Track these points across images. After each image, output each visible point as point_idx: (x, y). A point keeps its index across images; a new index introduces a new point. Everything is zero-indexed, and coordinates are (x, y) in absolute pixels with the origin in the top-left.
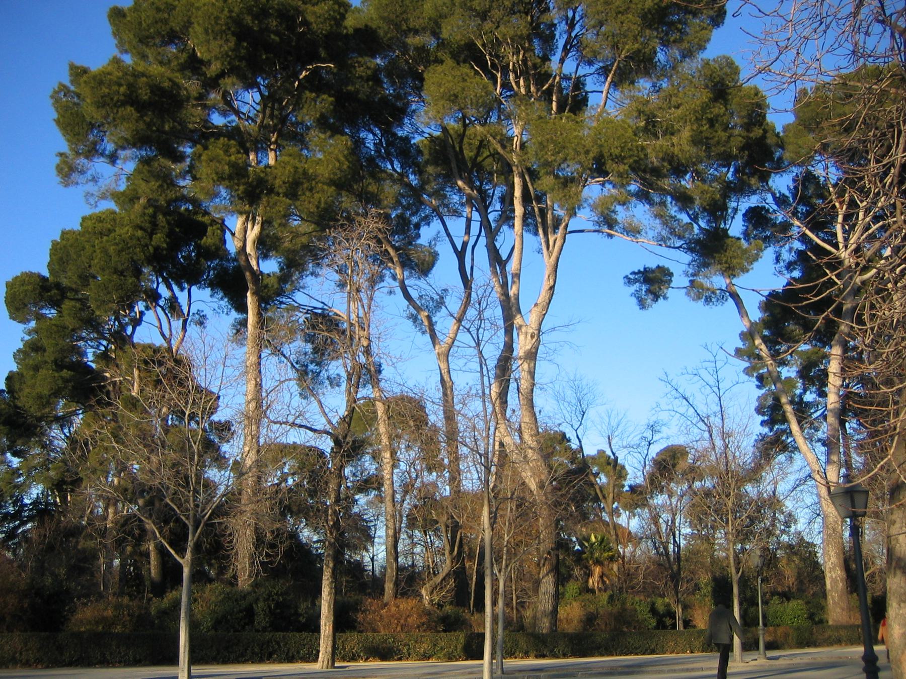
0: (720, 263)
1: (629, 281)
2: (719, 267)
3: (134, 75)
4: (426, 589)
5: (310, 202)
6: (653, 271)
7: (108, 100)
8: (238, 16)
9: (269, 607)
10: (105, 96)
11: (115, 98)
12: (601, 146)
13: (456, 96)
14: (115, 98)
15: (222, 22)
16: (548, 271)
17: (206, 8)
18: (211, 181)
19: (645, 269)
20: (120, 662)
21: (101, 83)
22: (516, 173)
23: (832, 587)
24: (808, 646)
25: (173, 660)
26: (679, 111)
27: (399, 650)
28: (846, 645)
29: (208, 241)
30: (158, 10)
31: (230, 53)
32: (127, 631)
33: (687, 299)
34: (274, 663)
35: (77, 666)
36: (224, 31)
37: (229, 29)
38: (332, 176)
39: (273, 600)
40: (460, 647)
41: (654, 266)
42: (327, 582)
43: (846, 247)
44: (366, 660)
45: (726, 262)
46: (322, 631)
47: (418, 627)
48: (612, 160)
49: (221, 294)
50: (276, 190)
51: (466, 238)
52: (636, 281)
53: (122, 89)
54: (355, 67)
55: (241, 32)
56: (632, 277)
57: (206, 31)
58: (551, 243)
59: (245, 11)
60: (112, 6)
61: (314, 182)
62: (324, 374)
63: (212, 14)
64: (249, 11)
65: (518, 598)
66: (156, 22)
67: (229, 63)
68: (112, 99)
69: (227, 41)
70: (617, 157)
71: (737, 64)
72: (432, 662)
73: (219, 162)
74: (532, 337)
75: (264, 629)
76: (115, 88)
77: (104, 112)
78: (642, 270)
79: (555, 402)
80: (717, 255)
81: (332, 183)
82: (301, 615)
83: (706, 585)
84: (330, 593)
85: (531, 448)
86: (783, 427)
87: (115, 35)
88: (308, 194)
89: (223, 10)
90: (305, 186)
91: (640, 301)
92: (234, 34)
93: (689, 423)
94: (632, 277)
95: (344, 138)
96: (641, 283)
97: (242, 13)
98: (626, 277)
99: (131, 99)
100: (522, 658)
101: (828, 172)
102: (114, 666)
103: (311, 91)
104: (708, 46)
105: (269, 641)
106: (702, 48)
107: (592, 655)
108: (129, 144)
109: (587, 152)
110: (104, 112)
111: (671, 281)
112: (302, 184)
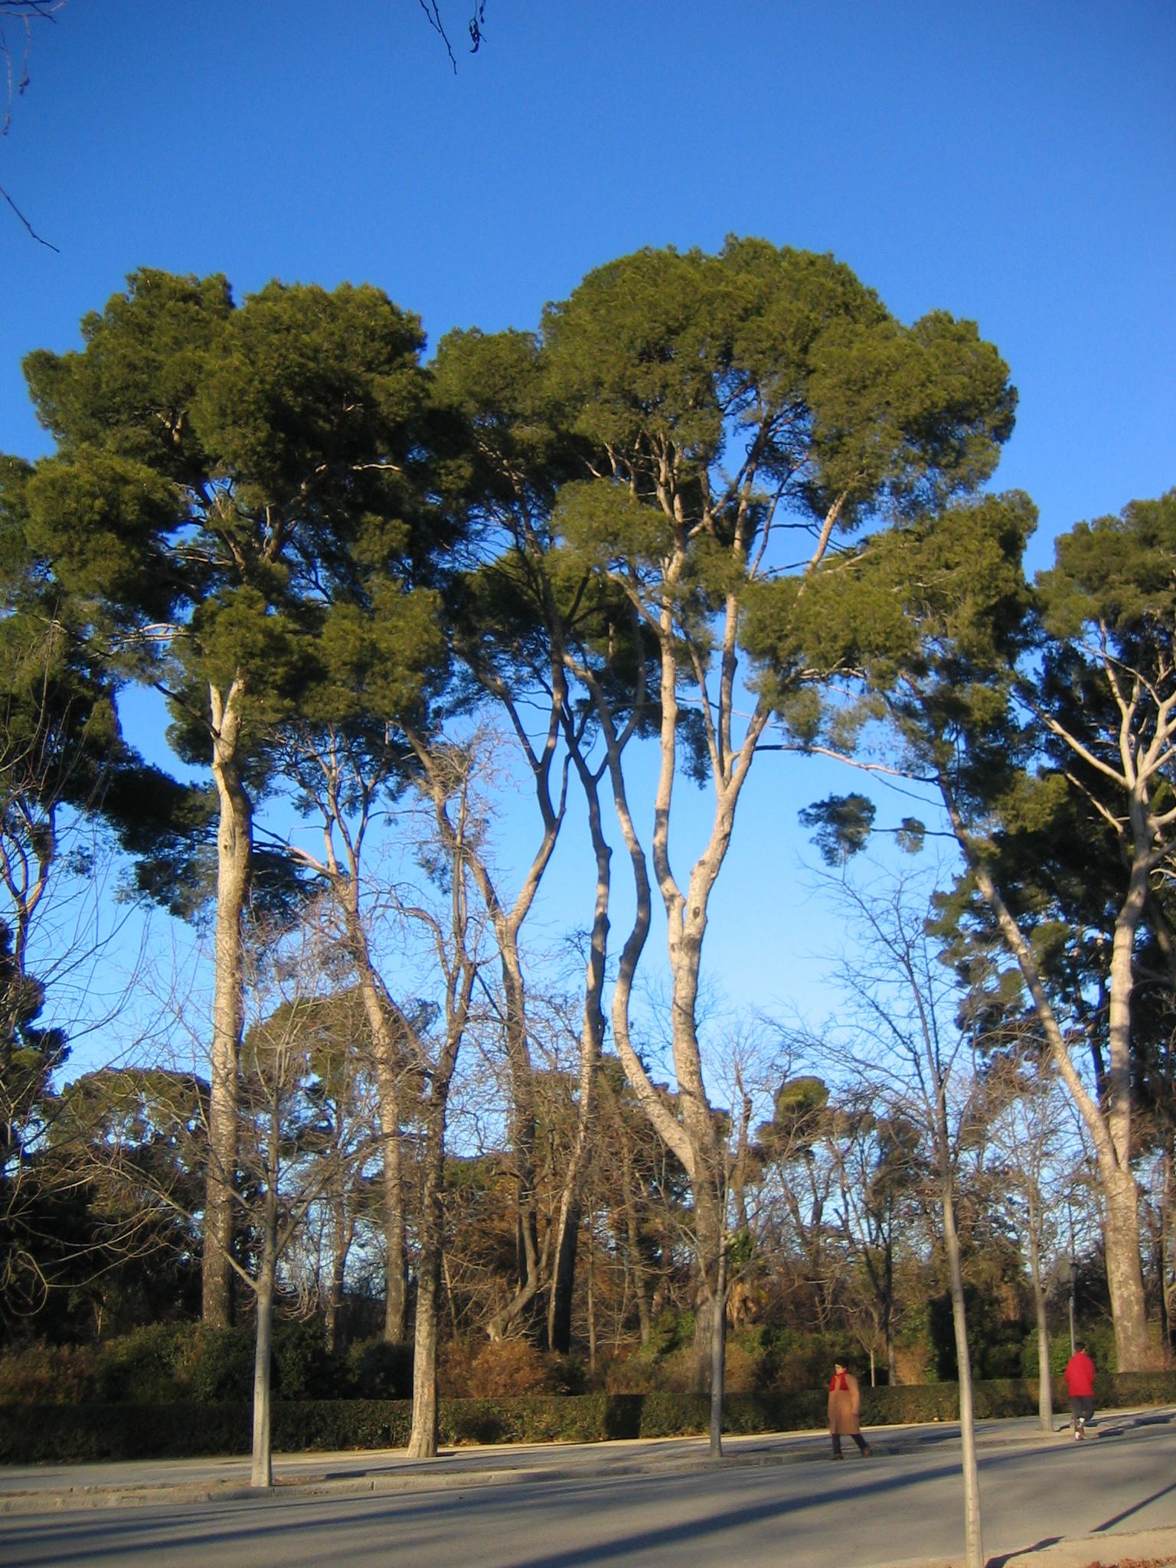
0: (1005, 809)
1: (808, 819)
2: (1003, 814)
3: (113, 480)
4: (495, 1326)
5: (384, 697)
6: (844, 803)
7: (74, 520)
8: (273, 389)
9: (304, 1357)
10: (71, 514)
11: (86, 518)
12: (855, 630)
13: (616, 535)
14: (86, 518)
15: (250, 397)
16: (721, 810)
17: (224, 373)
18: (233, 658)
19: (832, 798)
20: (75, 1456)
21: (64, 492)
22: (664, 649)
23: (1123, 1312)
24: (1107, 1407)
25: (244, 1448)
26: (954, 575)
27: (509, 1425)
28: (1160, 1403)
29: (91, 726)
30: (132, 367)
31: (259, 448)
32: (74, 1403)
33: (897, 848)
34: (317, 1451)
35: (7, 1463)
36: (252, 414)
37: (260, 410)
38: (416, 654)
39: (308, 1346)
40: (600, 1418)
41: (845, 795)
42: (425, 1316)
43: (1136, 774)
44: (457, 1443)
45: (1013, 808)
46: (415, 1396)
47: (532, 1387)
48: (871, 652)
49: (102, 820)
50: (331, 675)
51: (551, 743)
52: (818, 818)
53: (99, 503)
54: (440, 475)
55: (279, 416)
56: (813, 811)
57: (223, 413)
58: (727, 764)
59: (282, 381)
60: (35, 348)
61: (389, 664)
62: (269, 959)
63: (235, 385)
64: (290, 380)
65: (598, 1337)
66: (127, 387)
67: (257, 464)
68: (80, 519)
69: (256, 429)
70: (877, 648)
71: (1034, 503)
72: (557, 1445)
73: (249, 629)
74: (696, 914)
75: (297, 1396)
76: (87, 501)
77: (64, 538)
78: (826, 800)
79: (649, 1008)
80: (1001, 796)
81: (415, 666)
82: (349, 1370)
83: (919, 1312)
84: (430, 1334)
85: (690, 1094)
86: (1004, 1050)
87: (35, 396)
88: (380, 682)
89: (251, 380)
90: (376, 669)
91: (827, 852)
92: (267, 419)
93: (883, 1047)
94: (813, 811)
95: (431, 592)
96: (826, 822)
97: (276, 383)
98: (803, 811)
99: (109, 521)
100: (692, 1434)
101: (1097, 647)
102: (65, 1463)
103: (376, 512)
104: (994, 475)
105: (309, 1416)
106: (984, 476)
107: (795, 1428)
108: (104, 592)
109: (835, 638)
110: (64, 538)
111: (872, 819)
112: (372, 665)
